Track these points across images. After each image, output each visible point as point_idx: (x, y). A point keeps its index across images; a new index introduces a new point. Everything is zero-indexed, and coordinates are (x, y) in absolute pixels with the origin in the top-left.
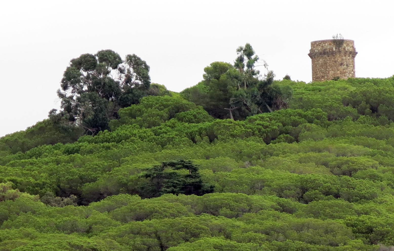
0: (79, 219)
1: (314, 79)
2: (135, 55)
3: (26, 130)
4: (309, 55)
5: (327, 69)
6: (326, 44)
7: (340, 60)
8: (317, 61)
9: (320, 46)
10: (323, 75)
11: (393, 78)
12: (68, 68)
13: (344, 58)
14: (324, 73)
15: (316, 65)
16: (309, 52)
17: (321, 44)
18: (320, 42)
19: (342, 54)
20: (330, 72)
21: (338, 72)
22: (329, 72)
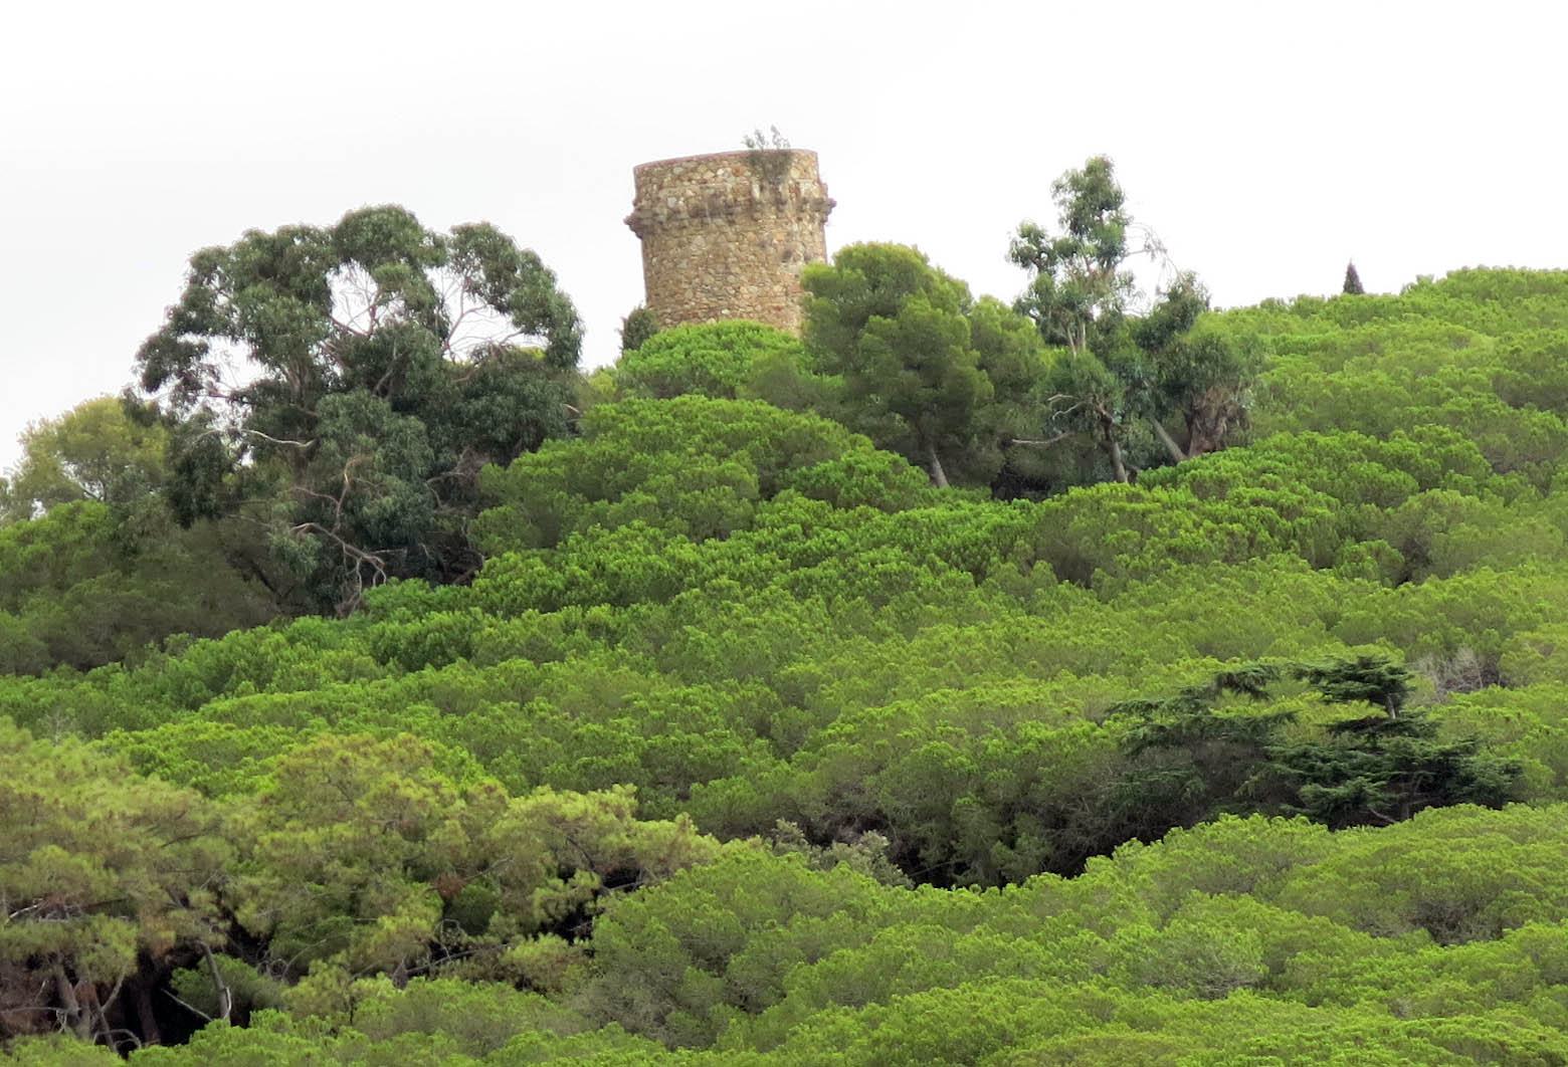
6: (720, 172)
9: (690, 180)
13: (795, 227)
14: (715, 295)
15: (676, 265)
16: (630, 210)
17: (694, 170)
18: (692, 165)
19: (789, 210)
21: (777, 288)
22: (737, 290)
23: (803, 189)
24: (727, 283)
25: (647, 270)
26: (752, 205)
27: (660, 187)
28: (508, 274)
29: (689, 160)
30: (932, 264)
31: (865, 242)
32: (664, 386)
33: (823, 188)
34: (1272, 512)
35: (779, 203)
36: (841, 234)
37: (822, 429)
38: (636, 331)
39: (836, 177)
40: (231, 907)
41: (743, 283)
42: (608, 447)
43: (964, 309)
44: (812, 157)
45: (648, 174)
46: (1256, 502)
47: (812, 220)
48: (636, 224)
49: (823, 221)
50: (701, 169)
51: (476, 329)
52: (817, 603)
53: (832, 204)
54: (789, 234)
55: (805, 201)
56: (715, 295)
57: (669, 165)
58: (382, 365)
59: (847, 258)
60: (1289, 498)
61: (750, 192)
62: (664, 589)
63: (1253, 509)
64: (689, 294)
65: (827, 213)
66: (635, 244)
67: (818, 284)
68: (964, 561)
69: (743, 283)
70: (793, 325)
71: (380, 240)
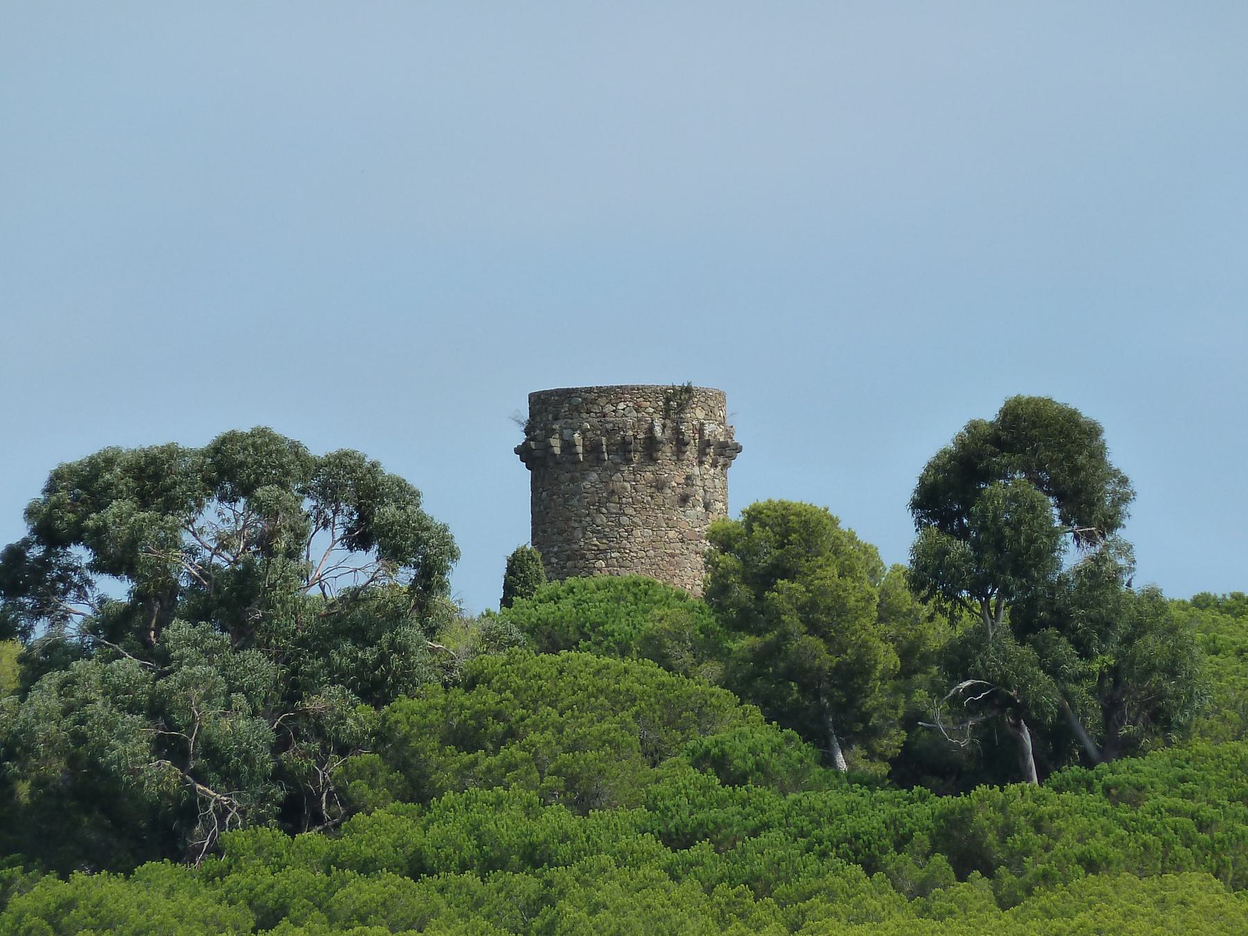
0: (86, 907)
1: (554, 560)
2: (1105, 436)
3: (1153, 596)
4: (517, 451)
5: (624, 520)
6: (621, 406)
7: (676, 478)
8: (572, 480)
9: (589, 412)
10: (602, 547)
11: (1239, 607)
12: (172, 452)
13: (696, 470)
14: (606, 537)
15: (566, 500)
16: (521, 438)
17: (594, 402)
18: (593, 396)
19: (691, 453)
20: (637, 532)
21: (672, 534)
22: (630, 532)
23: (708, 429)
24: (620, 525)
25: (534, 504)
26: (651, 445)
27: (556, 419)
28: (375, 509)
29: (590, 390)
30: (844, 526)
31: (776, 500)
32: (550, 639)
33: (729, 434)
34: (1187, 823)
35: (680, 444)
36: (744, 490)
37: (712, 695)
38: (517, 578)
39: (742, 420)
40: (294, 914)
41: (635, 525)
42: (491, 698)
43: (873, 573)
44: (720, 397)
45: (544, 402)
46: (1173, 811)
47: (714, 465)
48: (524, 452)
49: (725, 466)
50: (602, 401)
51: (335, 566)
52: (690, 885)
53: (738, 449)
54: (688, 478)
55: (708, 444)
56: (606, 537)
57: (568, 394)
58: (235, 601)
59: (754, 516)
60: (1208, 812)
61: (651, 429)
62: (534, 857)
63: (1170, 820)
64: (578, 534)
65: (732, 458)
66: (524, 475)
67: (724, 541)
68: (856, 852)
69: (635, 525)
70: (692, 579)
71: (237, 466)
